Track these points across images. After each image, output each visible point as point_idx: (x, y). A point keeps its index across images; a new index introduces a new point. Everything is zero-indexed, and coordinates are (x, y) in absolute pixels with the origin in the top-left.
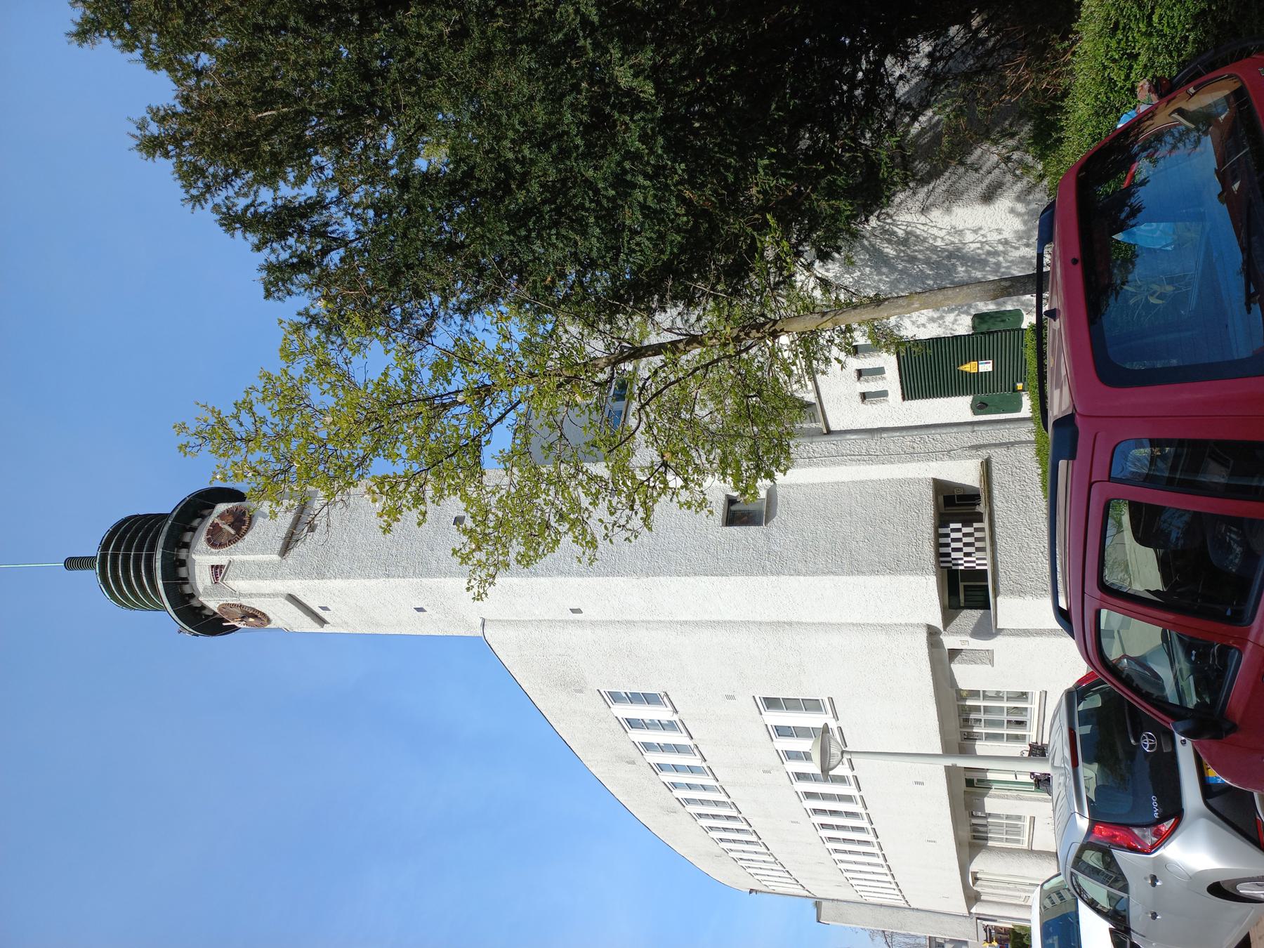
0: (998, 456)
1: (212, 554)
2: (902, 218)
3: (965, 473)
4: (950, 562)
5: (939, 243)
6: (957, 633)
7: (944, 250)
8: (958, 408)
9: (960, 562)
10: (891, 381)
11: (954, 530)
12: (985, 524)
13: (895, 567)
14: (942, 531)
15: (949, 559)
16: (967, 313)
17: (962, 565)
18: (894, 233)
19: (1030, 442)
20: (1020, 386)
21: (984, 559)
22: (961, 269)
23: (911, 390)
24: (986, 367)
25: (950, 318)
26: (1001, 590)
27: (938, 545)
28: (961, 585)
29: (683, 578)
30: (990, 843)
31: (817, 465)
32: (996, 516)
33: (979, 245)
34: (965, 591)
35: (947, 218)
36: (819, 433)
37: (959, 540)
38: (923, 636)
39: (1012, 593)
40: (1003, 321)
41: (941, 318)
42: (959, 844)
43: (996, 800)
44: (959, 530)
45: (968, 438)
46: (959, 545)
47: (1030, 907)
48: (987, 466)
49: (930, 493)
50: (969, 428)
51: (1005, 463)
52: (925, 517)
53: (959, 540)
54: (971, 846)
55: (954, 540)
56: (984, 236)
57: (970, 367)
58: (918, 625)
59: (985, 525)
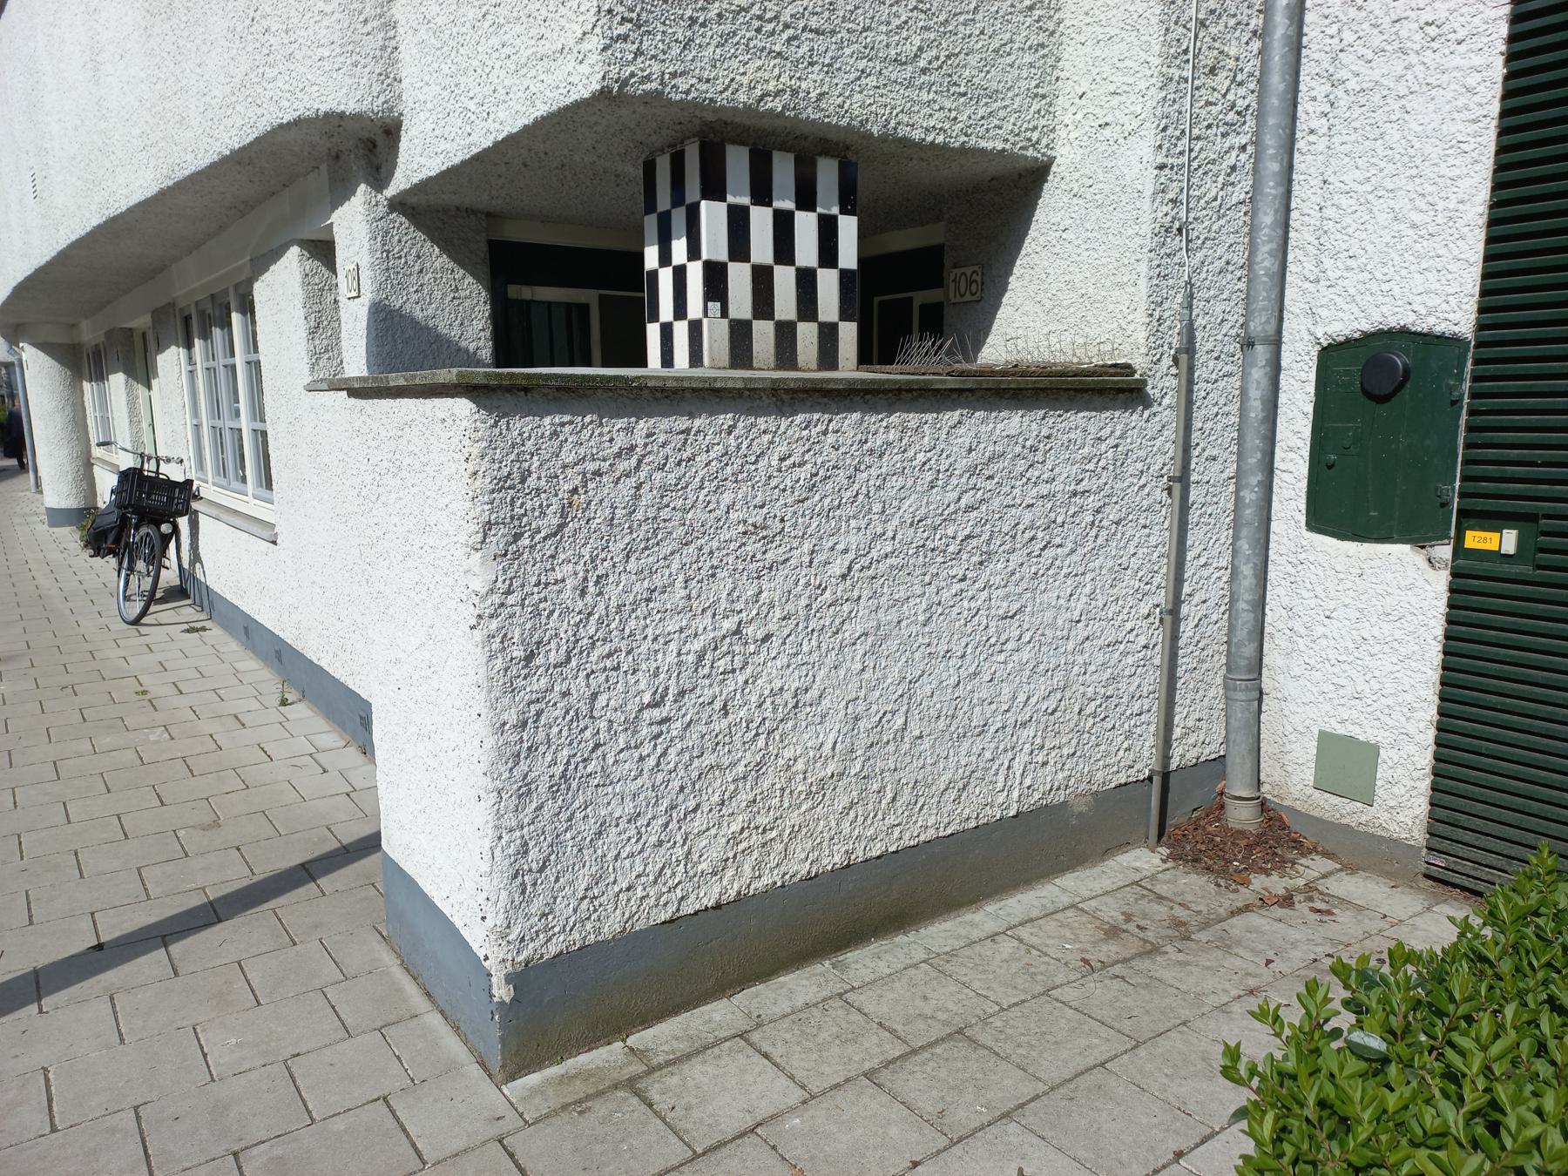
4: (678, 197)
6: (386, 255)
9: (679, 249)
14: (827, 175)
15: (693, 190)
17: (665, 259)
21: (696, 357)
26: (521, 425)
28: (589, 296)
32: (913, 419)
34: (568, 307)
37: (784, 248)
39: (502, 484)
44: (828, 254)
46: (762, 247)
51: (1120, 463)
52: (897, 97)
53: (784, 248)
55: (783, 228)
58: (390, 79)
59: (848, 368)
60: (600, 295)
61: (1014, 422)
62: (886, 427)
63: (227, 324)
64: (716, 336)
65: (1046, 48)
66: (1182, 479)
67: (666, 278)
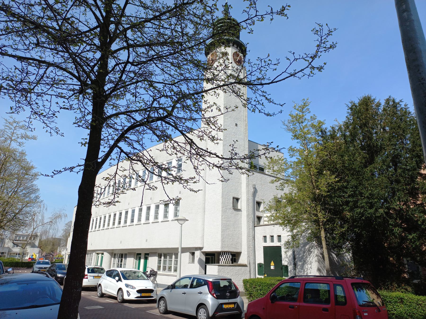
0: (248, 269)
1: (231, 54)
2: (316, 251)
3: (243, 260)
4: (222, 255)
5: (308, 259)
7: (306, 260)
8: (260, 259)
9: (222, 257)
10: (269, 244)
11: (230, 256)
12: (231, 264)
13: (223, 241)
14: (230, 253)
15: (223, 254)
16: (288, 264)
18: (312, 249)
19: (250, 277)
20: (266, 275)
21: (223, 263)
22: (301, 263)
23: (267, 250)
24: (272, 267)
25: (287, 260)
27: (227, 252)
29: (221, 186)
30: (113, 259)
31: (247, 223)
33: (307, 268)
35: (314, 261)
36: (254, 225)
38: (201, 246)
40: (285, 272)
41: (287, 258)
42: (113, 250)
43: (133, 261)
44: (230, 258)
45: (252, 262)
47: (121, 267)
48: (245, 266)
49: (238, 251)
50: (254, 262)
51: (246, 270)
54: (112, 253)
56: (309, 269)
57: (272, 263)
58: (203, 245)
60: (178, 248)
61: (240, 267)
62: (233, 267)
63: (171, 258)
64: (224, 262)
65: (241, 246)
66: (250, 271)
67: (221, 259)
